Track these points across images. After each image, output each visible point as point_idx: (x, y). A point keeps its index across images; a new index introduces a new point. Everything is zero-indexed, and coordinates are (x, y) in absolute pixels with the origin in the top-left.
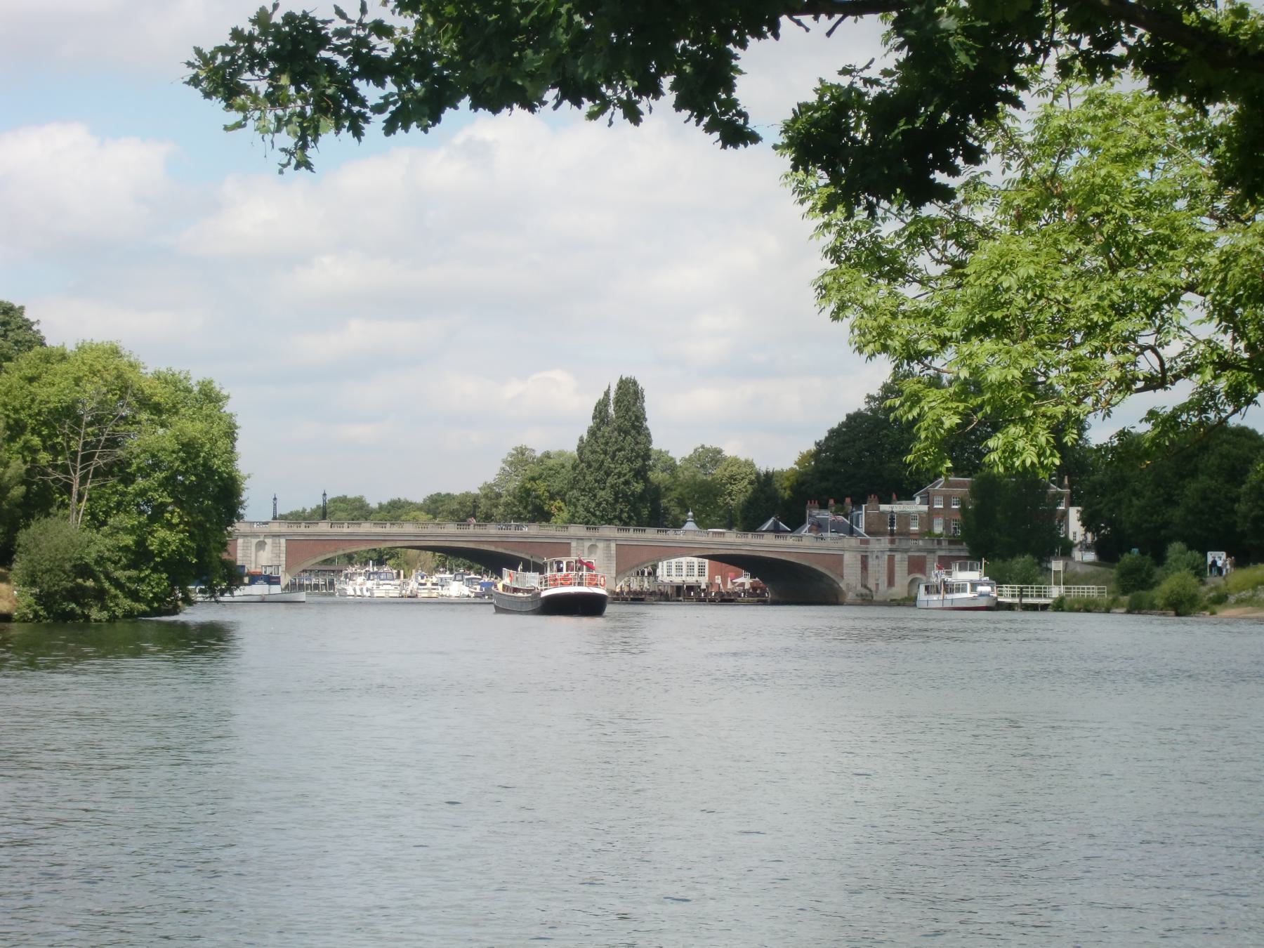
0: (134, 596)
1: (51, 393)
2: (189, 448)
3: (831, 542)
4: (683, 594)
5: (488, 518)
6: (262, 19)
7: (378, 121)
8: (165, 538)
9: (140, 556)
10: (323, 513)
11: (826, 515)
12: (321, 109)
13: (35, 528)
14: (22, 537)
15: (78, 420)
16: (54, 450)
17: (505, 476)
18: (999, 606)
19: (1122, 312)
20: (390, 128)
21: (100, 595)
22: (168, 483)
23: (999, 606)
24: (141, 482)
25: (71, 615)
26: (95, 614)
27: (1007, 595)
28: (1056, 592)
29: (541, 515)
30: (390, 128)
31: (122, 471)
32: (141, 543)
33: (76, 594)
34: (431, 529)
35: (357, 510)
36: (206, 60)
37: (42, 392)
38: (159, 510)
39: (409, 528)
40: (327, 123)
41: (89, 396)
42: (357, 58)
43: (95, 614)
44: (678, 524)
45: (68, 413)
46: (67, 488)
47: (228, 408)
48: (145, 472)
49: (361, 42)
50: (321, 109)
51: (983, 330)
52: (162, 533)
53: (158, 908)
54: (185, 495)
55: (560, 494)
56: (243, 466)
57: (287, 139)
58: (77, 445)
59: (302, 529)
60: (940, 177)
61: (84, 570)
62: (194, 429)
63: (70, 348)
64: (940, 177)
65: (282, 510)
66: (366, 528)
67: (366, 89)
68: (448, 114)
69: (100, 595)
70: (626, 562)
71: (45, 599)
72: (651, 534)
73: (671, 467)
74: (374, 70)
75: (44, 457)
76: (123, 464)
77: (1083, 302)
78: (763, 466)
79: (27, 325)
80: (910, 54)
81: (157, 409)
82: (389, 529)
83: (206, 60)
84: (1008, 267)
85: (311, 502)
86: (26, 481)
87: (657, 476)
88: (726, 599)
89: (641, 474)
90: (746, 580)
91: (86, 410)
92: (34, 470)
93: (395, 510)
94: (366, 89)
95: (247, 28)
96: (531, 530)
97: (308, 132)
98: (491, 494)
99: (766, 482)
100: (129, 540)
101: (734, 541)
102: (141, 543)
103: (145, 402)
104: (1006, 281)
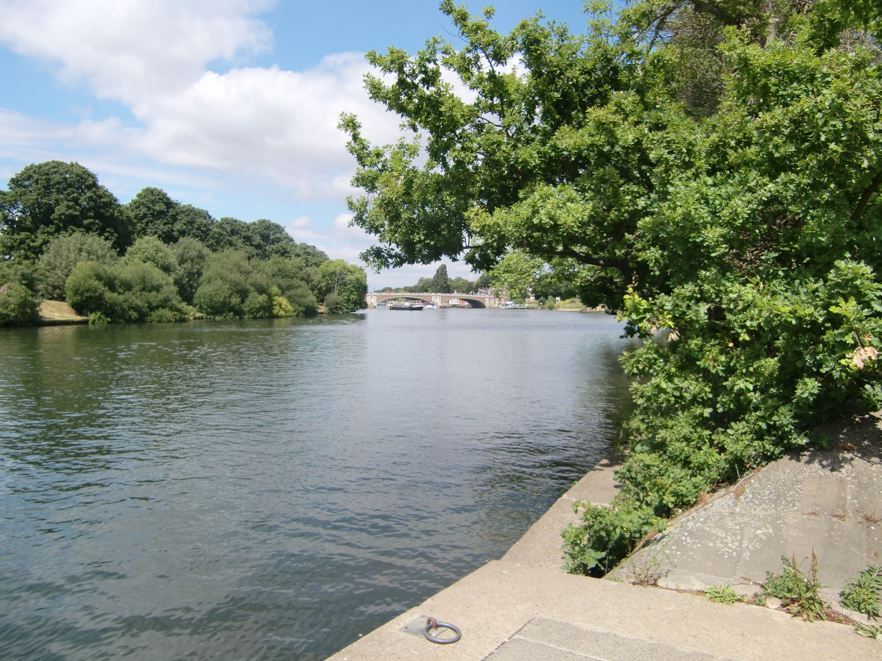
0: (347, 309)
1: (331, 269)
2: (358, 280)
3: (483, 295)
4: (454, 306)
5: (415, 292)
6: (372, 248)
7: (392, 266)
8: (353, 297)
9: (348, 301)
10: (383, 291)
11: (482, 290)
12: (382, 264)
13: (328, 296)
14: (326, 297)
15: (336, 274)
16: (332, 280)
17: (419, 283)
18: (516, 308)
19: (533, 267)
20: (394, 267)
21: (341, 308)
22: (353, 286)
23: (516, 308)
24: (348, 286)
25: (335, 312)
26: (340, 312)
27: (517, 306)
28: (527, 305)
29: (426, 291)
30: (394, 267)
31: (345, 284)
32: (349, 298)
33: (336, 308)
34: (405, 294)
35: (389, 290)
36: (363, 254)
37: (329, 269)
38: (352, 292)
39: (400, 294)
40: (383, 266)
41: (338, 270)
42: (388, 254)
43: (340, 312)
44: (453, 292)
45: (334, 273)
46: (334, 288)
47: (365, 272)
48: (349, 284)
49: (389, 252)
50: (382, 264)
51: (507, 272)
52: (352, 296)
53: (363, 471)
54: (357, 289)
55: (430, 287)
56: (368, 283)
57: (376, 269)
58: (336, 279)
59: (380, 294)
60: (492, 266)
61: (337, 304)
62: (358, 276)
63: (334, 260)
64: (492, 266)
65: (376, 290)
66: (392, 294)
67: (390, 260)
68: (404, 264)
69: (341, 308)
70: (443, 299)
71: (330, 309)
72: (448, 295)
73: (452, 281)
74: (391, 256)
75: (330, 282)
76: (345, 283)
77: (526, 266)
78: (470, 281)
79: (326, 255)
80: (360, 635)
81: (351, 272)
82: (397, 294)
83: (363, 254)
84: (511, 260)
85: (381, 288)
86: (326, 286)
87: (449, 283)
88: (462, 307)
89: (446, 283)
90: (466, 303)
91: (338, 273)
92: (328, 284)
93: (397, 290)
94: (390, 260)
95: (369, 249)
96: (425, 294)
97: (379, 268)
98: (416, 287)
99: (471, 284)
100: (346, 298)
101: (464, 296)
102: (349, 298)
103: (349, 271)
104: (511, 263)
